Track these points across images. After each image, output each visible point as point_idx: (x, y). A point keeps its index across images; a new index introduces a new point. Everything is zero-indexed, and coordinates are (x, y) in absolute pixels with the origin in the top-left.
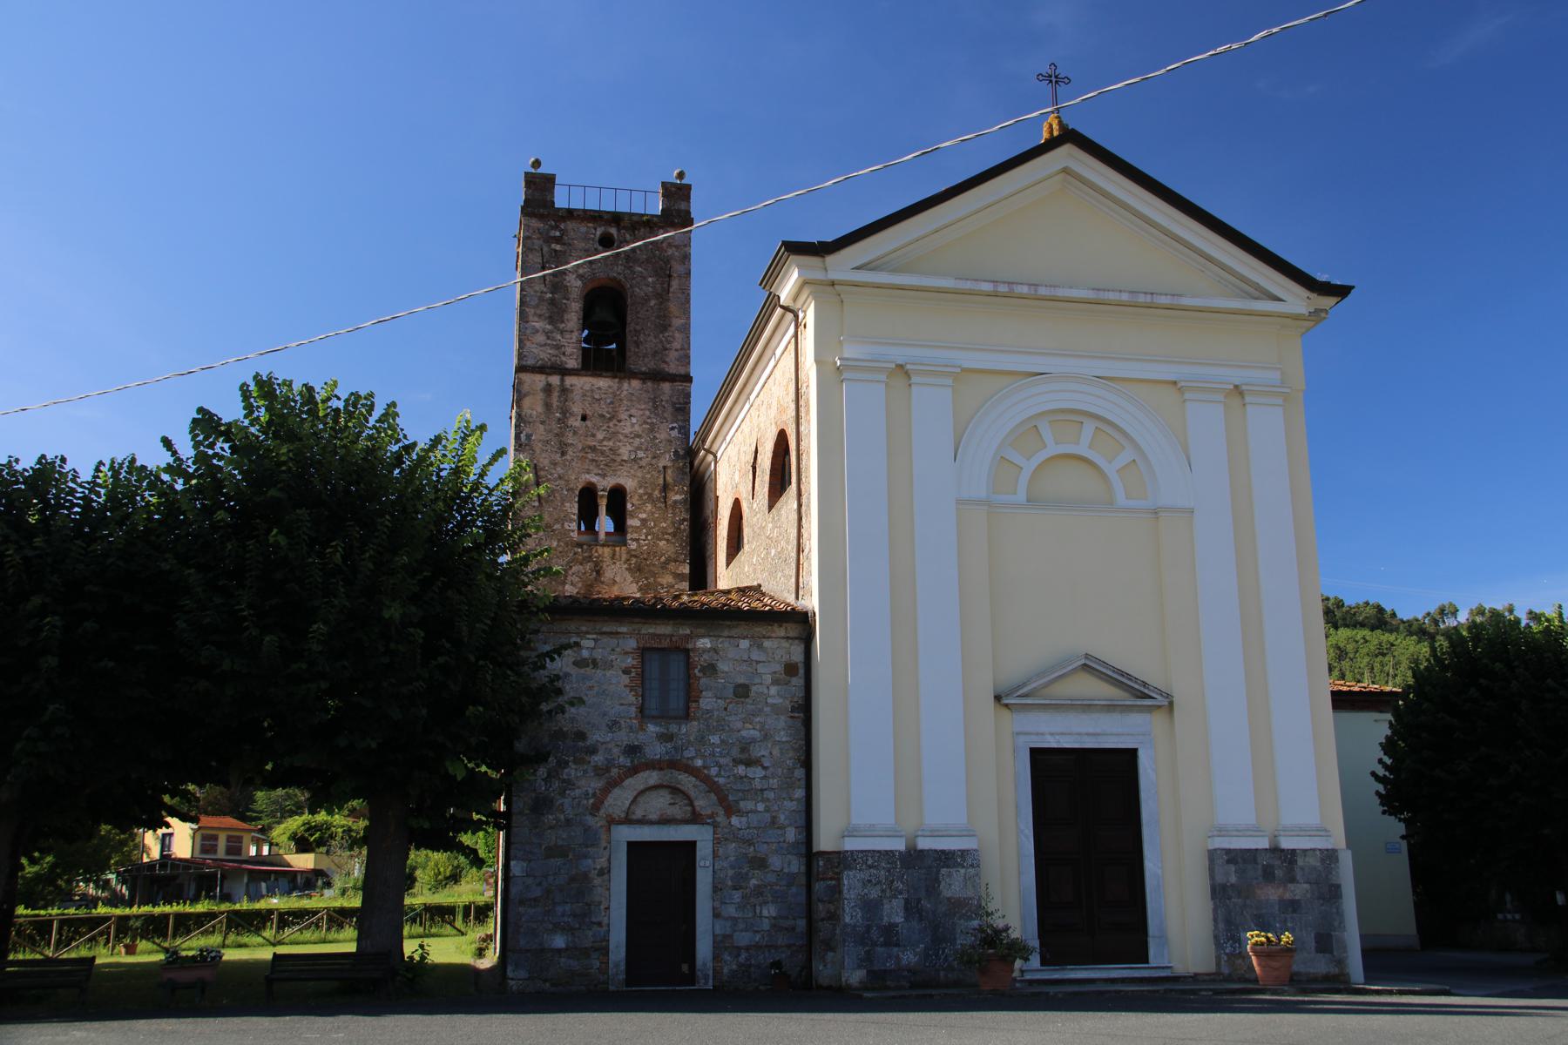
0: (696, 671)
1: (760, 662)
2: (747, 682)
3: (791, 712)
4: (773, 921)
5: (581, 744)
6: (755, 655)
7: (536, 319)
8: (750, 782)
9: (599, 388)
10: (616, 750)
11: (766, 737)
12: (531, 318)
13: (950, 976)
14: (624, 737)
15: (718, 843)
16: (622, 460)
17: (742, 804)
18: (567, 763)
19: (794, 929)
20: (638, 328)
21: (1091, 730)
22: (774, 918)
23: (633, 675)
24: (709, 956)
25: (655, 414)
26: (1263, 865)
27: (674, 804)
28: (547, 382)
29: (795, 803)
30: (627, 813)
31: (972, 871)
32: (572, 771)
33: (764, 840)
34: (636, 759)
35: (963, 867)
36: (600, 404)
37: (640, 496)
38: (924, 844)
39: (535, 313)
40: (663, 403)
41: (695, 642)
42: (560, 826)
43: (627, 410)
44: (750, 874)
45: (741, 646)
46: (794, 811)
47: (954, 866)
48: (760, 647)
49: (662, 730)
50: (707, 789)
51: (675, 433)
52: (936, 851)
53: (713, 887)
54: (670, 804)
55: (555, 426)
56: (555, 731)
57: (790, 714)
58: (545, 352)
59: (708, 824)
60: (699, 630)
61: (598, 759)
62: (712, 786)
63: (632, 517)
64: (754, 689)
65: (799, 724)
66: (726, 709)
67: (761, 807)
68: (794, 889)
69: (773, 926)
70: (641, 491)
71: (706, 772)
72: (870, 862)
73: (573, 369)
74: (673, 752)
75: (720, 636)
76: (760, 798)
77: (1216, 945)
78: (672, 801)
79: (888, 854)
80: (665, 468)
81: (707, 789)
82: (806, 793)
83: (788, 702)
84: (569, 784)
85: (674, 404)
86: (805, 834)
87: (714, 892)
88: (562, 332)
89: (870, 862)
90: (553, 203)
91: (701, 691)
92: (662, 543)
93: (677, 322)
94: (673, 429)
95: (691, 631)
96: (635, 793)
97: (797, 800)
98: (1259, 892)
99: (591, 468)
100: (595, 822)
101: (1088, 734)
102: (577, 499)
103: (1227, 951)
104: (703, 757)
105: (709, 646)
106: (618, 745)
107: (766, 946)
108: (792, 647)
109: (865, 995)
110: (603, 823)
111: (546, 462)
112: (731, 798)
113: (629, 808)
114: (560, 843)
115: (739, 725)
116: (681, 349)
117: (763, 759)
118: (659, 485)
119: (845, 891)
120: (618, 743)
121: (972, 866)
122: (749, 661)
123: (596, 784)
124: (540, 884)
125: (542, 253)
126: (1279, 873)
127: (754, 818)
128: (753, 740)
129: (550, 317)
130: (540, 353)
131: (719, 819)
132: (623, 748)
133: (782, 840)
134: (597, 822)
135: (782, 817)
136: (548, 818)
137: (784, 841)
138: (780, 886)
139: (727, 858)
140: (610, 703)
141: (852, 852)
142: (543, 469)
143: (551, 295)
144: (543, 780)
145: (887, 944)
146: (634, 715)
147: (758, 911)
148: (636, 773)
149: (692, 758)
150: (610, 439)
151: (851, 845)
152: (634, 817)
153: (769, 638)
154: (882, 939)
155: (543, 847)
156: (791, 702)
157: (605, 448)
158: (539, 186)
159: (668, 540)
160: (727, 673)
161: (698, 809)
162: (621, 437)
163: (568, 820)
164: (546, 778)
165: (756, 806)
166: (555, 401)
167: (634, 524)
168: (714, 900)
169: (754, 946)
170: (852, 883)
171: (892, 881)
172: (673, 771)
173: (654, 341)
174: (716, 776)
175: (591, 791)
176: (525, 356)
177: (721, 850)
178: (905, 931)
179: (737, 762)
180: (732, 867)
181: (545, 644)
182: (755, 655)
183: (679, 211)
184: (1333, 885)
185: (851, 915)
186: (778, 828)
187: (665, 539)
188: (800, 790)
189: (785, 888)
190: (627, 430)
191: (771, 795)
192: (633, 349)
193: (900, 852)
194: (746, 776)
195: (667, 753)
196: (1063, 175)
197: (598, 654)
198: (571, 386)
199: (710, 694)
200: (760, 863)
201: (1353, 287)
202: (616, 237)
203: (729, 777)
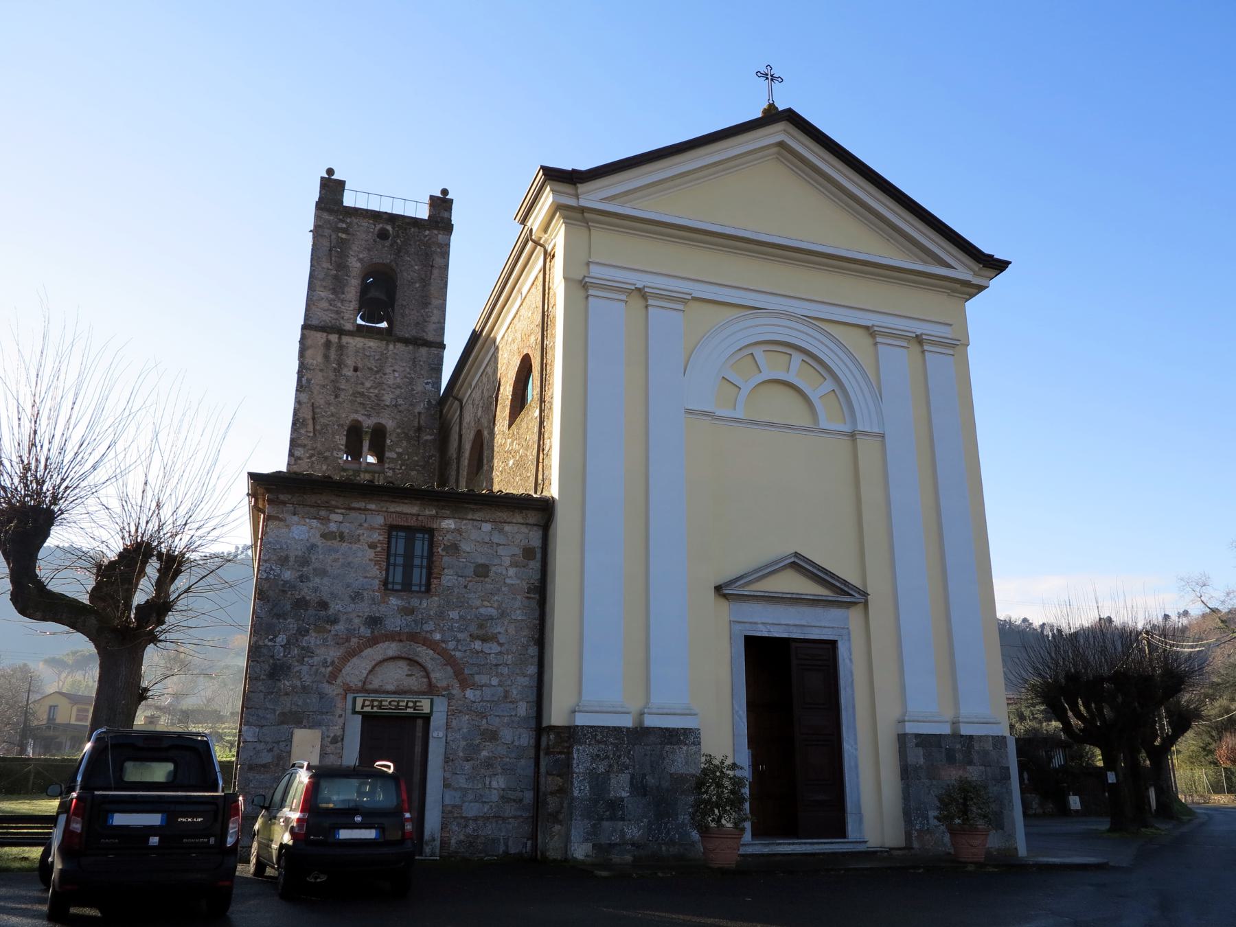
0: (440, 549)
1: (500, 545)
2: (487, 562)
3: (528, 593)
5: (322, 613)
6: (496, 538)
7: (322, 289)
8: (486, 657)
9: (370, 347)
10: (356, 621)
11: (503, 614)
12: (318, 289)
13: (671, 850)
14: (365, 609)
16: (385, 405)
17: (477, 678)
18: (307, 631)
19: (521, 800)
20: (405, 303)
21: (797, 623)
22: (503, 790)
23: (379, 549)
24: (437, 826)
25: (414, 371)
26: (947, 748)
27: (411, 675)
28: (327, 339)
29: (527, 679)
30: (364, 683)
31: (693, 748)
32: (312, 639)
33: (496, 714)
34: (376, 629)
35: (686, 744)
36: (369, 359)
37: (398, 434)
38: (650, 722)
39: (321, 285)
40: (421, 363)
41: (440, 523)
42: (297, 693)
43: (391, 366)
44: (482, 746)
45: (483, 529)
46: (526, 686)
47: (678, 743)
48: (501, 531)
49: (403, 603)
50: (445, 662)
51: (429, 387)
53: (445, 758)
54: (407, 675)
55: (332, 376)
56: (297, 599)
57: (527, 595)
58: (327, 315)
59: (443, 696)
60: (443, 511)
61: (340, 627)
62: (449, 660)
63: (391, 450)
64: (493, 569)
65: (534, 604)
66: (466, 587)
67: (495, 681)
68: (523, 761)
69: (502, 797)
70: (399, 431)
71: (444, 645)
73: (349, 331)
74: (413, 625)
75: (463, 519)
77: (905, 822)
78: (410, 673)
80: (419, 413)
82: (538, 670)
83: (524, 583)
84: (308, 651)
85: (430, 364)
86: (535, 709)
87: (446, 762)
88: (342, 301)
89: (598, 738)
90: (343, 202)
91: (444, 569)
92: (413, 473)
93: (435, 302)
94: (427, 383)
95: (437, 512)
96: (374, 663)
97: (531, 676)
99: (359, 409)
100: (331, 690)
102: (345, 433)
103: (917, 828)
104: (442, 632)
105: (453, 526)
106: (359, 616)
107: (494, 817)
108: (531, 533)
109: (596, 872)
110: (341, 691)
111: (322, 402)
112: (466, 671)
113: (366, 678)
114: (294, 708)
115: (478, 603)
116: (438, 323)
117: (500, 637)
118: (414, 427)
119: (575, 766)
120: (360, 614)
121: (693, 743)
122: (491, 544)
123: (334, 653)
124: (271, 750)
125: (330, 239)
126: (959, 756)
127: (488, 692)
128: (491, 618)
129: (334, 289)
130: (326, 317)
131: (454, 692)
132: (364, 619)
133: (513, 714)
134: (333, 691)
135: (515, 692)
136: (284, 684)
137: (516, 715)
138: (510, 759)
139: (459, 730)
140: (354, 575)
141: (582, 727)
142: (319, 407)
143: (335, 272)
144: (282, 646)
145: (613, 818)
146: (377, 588)
147: (487, 783)
148: (375, 644)
149: (431, 632)
150: (376, 388)
151: (581, 720)
152: (371, 687)
153: (509, 523)
154: (608, 813)
155: (277, 713)
156: (528, 583)
157: (371, 395)
158: (331, 188)
159: (418, 471)
160: (468, 553)
161: (434, 681)
162: (385, 387)
163: (304, 687)
164: (286, 644)
165: (490, 680)
166: (333, 354)
167: (391, 456)
168: (445, 771)
169: (482, 817)
170: (581, 758)
171: (619, 757)
172: (412, 643)
173: (417, 314)
174: (454, 650)
175: (329, 660)
176: (310, 317)
177: (454, 723)
178: (630, 806)
179: (473, 637)
180: (464, 738)
181: (295, 515)
182: (496, 538)
183: (443, 218)
185: (580, 789)
186: (510, 702)
187: (416, 470)
188: (533, 667)
189: (515, 760)
190: (391, 382)
191: (505, 671)
192: (399, 319)
193: (628, 729)
194: (482, 651)
195: (407, 625)
196: (775, 150)
197: (346, 529)
198: (347, 343)
199: (451, 572)
200: (493, 736)
201: (1010, 263)
202: (391, 232)
203: (465, 651)
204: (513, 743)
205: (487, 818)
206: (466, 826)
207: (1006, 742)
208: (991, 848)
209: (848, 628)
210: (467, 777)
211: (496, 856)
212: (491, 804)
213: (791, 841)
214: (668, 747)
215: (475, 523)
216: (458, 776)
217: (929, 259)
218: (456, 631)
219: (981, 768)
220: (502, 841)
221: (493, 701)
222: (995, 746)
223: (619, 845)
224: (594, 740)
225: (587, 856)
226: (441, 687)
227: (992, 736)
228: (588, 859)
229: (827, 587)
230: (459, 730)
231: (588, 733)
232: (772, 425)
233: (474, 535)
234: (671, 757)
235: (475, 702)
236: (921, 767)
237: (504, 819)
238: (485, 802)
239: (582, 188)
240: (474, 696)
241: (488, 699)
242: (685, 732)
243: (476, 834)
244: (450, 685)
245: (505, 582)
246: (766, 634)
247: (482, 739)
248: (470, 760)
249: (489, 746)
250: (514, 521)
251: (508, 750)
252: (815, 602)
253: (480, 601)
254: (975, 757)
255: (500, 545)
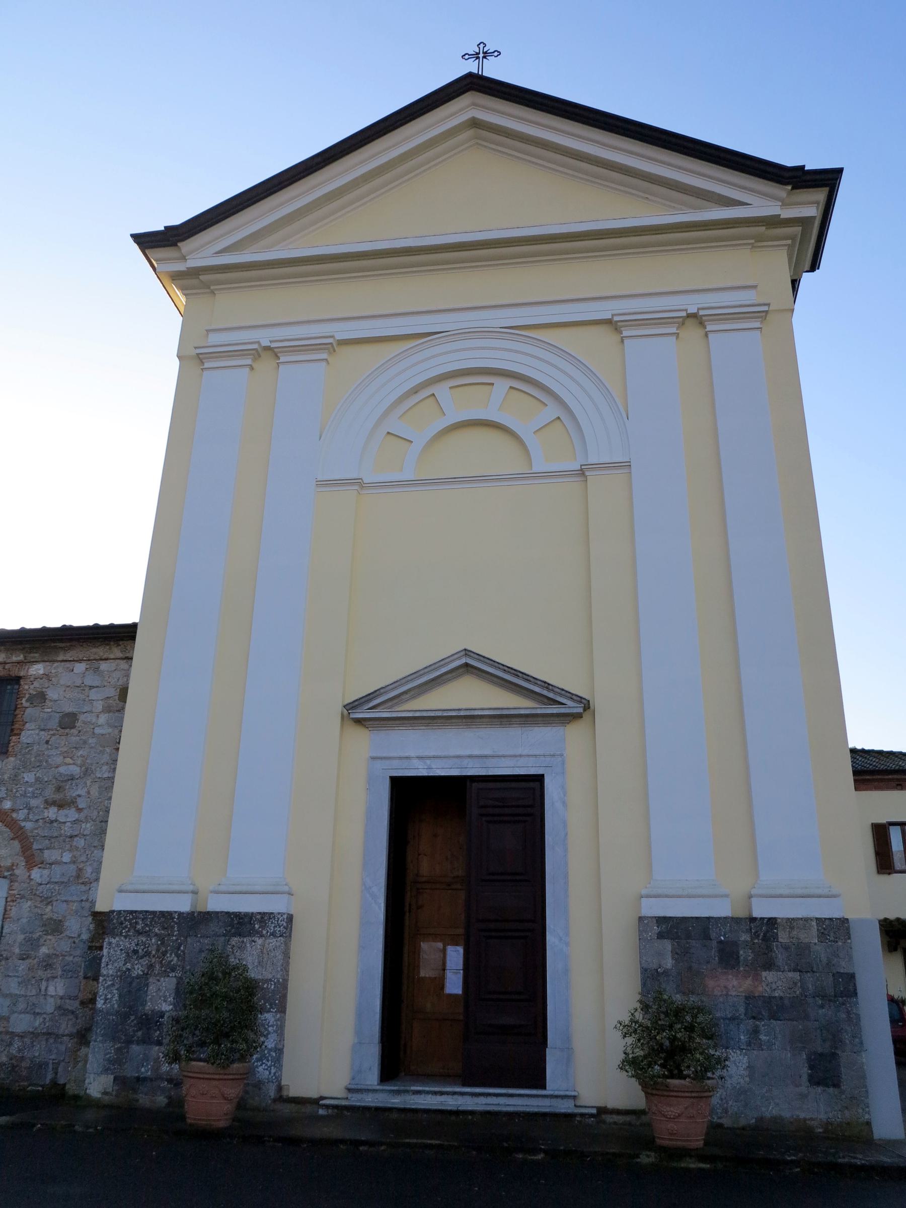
1: (94, 687)
4: (59, 1001)
15: (13, 901)
17: (47, 853)
21: (477, 752)
22: (61, 998)
26: (721, 942)
33: (64, 899)
35: (262, 936)
44: (42, 941)
47: (250, 935)
48: (97, 670)
50: (12, 835)
52: (227, 913)
59: (4, 877)
60: (32, 655)
64: (82, 717)
66: (47, 742)
72: (139, 927)
76: (68, 847)
79: (165, 916)
81: (12, 835)
89: (139, 927)
95: (25, 657)
98: (711, 983)
101: (470, 756)
105: (41, 672)
115: (59, 760)
117: (79, 800)
126: (745, 954)
131: (17, 872)
133: (84, 898)
139: (18, 919)
147: (43, 988)
153: (106, 659)
154: (140, 1033)
160: (56, 701)
169: (32, 1033)
171: (166, 952)
174: (24, 820)
179: (49, 803)
180: (23, 931)
182: (90, 680)
184: (841, 975)
193: (180, 914)
194: (56, 821)
196: (471, 132)
200: (55, 927)
203: (37, 821)
204: (79, 936)
205: (34, 1035)
206: (10, 1044)
207: (848, 929)
208: (811, 1119)
209: (562, 755)
210: (20, 980)
211: (41, 1086)
212: (45, 1016)
213: (437, 1089)
214: (235, 940)
215: (68, 665)
216: (10, 979)
217: (699, 202)
218: (29, 797)
219: (791, 974)
220: (51, 1066)
221: (63, 883)
222: (822, 935)
223: (151, 1080)
224: (132, 931)
225: (105, 1093)
226: (4, 866)
227: (817, 919)
228: (107, 1098)
229: (534, 699)
230: (18, 919)
231: (125, 919)
232: (454, 480)
233: (65, 679)
234: (237, 954)
235: (41, 884)
236: (666, 973)
237: (57, 1036)
238: (38, 1014)
239: (186, 246)
240: (41, 876)
241: (56, 880)
242: (262, 918)
243: (21, 1055)
244: (15, 864)
245: (93, 732)
246: (424, 773)
247: (43, 931)
248: (27, 958)
249: (50, 940)
250: (112, 656)
251: (73, 945)
252: (502, 719)
253: (62, 757)
254: (780, 957)
255: (94, 687)
